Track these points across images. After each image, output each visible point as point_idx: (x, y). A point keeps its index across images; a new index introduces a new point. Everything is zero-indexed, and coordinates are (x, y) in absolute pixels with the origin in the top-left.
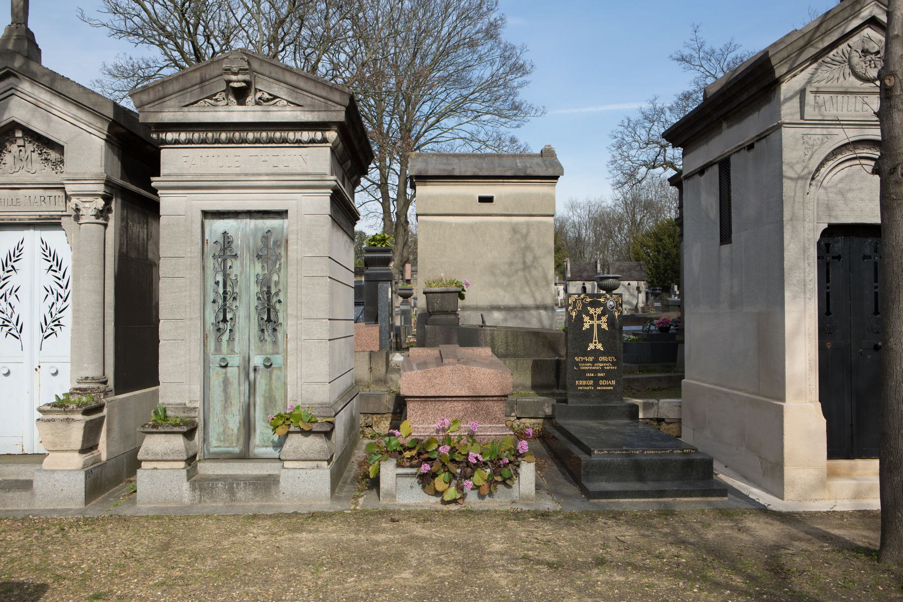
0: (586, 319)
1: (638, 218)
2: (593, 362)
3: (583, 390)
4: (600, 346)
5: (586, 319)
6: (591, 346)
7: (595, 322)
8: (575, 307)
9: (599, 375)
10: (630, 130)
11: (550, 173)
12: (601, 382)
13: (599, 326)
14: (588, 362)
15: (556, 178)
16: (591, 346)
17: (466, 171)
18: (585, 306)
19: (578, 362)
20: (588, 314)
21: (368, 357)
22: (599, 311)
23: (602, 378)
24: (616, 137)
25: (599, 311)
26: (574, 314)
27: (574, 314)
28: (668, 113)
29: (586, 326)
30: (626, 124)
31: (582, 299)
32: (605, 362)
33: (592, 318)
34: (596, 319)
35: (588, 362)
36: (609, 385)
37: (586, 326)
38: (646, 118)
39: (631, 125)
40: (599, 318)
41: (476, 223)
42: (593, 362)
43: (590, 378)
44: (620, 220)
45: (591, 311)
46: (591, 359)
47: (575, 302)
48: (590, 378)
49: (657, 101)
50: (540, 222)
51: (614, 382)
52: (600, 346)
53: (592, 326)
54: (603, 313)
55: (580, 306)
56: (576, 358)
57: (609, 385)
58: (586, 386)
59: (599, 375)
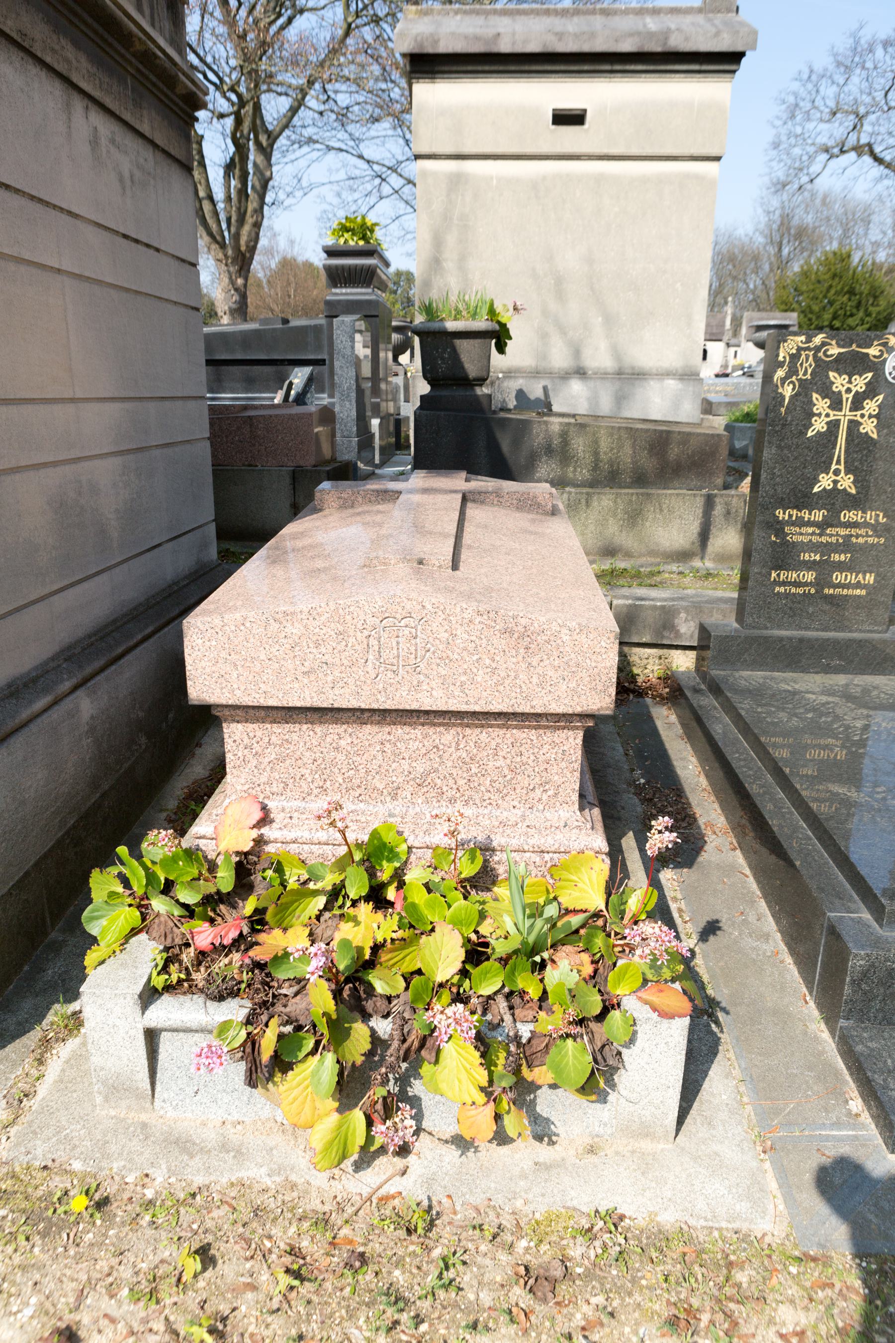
0: (821, 405)
1: (785, 251)
2: (823, 526)
3: (787, 595)
4: (847, 482)
5: (821, 405)
6: (825, 482)
7: (845, 416)
8: (792, 371)
9: (836, 557)
10: (810, 86)
11: (723, 44)
12: (838, 577)
13: (854, 425)
14: (809, 524)
15: (733, 58)
16: (825, 482)
17: (526, 42)
18: (822, 367)
19: (783, 523)
20: (826, 391)
21: (288, 480)
22: (860, 383)
23: (841, 567)
24: (784, 102)
25: (860, 383)
26: (788, 391)
27: (788, 391)
28: (879, 52)
29: (819, 425)
30: (805, 76)
31: (817, 349)
32: (855, 525)
33: (836, 404)
34: (847, 406)
35: (809, 524)
36: (858, 585)
37: (819, 425)
38: (839, 64)
39: (814, 78)
40: (857, 403)
41: (544, 178)
42: (823, 526)
43: (810, 566)
44: (756, 258)
45: (839, 382)
46: (818, 515)
47: (794, 357)
48: (810, 566)
49: (862, 33)
50: (688, 176)
51: (870, 578)
52: (847, 482)
53: (834, 426)
54: (826, 391)
55: (806, 368)
56: (780, 514)
57: (858, 585)
58: (797, 584)
59: (836, 557)
